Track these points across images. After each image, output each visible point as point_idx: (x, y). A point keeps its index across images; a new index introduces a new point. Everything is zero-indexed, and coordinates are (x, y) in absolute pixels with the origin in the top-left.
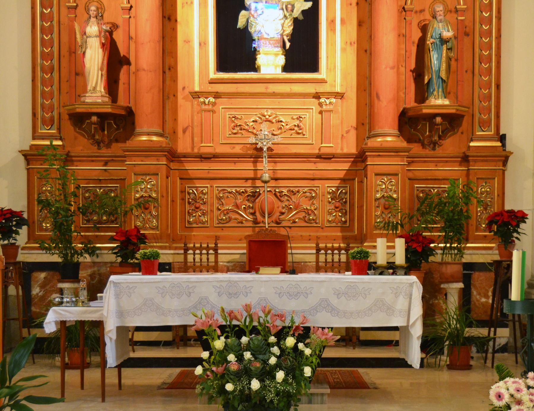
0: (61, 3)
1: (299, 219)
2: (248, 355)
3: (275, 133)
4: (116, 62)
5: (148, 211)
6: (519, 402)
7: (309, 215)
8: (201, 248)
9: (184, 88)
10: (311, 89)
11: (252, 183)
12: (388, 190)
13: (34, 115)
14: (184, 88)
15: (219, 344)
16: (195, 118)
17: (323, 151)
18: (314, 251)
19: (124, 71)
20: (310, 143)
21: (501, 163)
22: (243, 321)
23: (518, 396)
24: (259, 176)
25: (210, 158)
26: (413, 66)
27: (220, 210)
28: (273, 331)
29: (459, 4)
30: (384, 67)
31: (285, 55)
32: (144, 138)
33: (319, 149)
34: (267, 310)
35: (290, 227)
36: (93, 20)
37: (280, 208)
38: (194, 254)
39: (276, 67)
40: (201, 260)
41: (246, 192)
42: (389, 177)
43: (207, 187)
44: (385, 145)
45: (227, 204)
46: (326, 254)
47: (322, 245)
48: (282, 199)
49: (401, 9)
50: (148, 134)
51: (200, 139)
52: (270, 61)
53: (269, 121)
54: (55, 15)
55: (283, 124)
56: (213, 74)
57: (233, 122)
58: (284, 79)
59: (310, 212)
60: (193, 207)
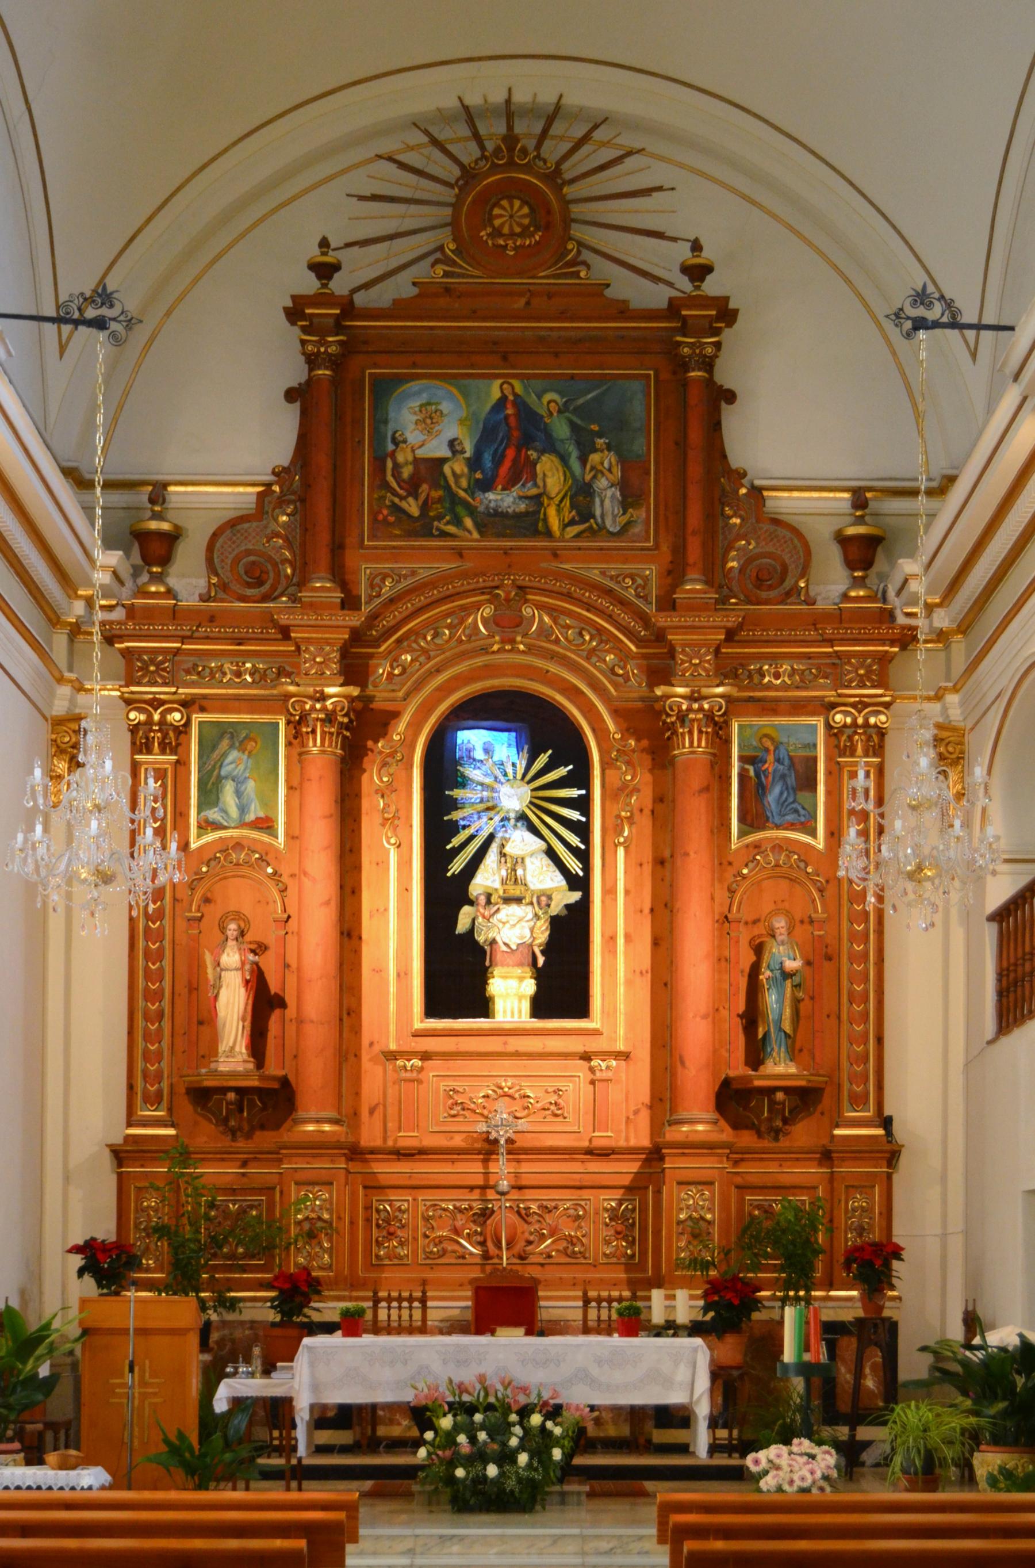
0: (177, 913)
1: (558, 1251)
2: (482, 1436)
3: (518, 1115)
4: (264, 1001)
5: (314, 1242)
6: (778, 1468)
7: (574, 1245)
8: (400, 1299)
9: (371, 1044)
10: (577, 1045)
11: (481, 1194)
12: (699, 1208)
13: (131, 1087)
14: (371, 1044)
15: (446, 1422)
16: (390, 1091)
17: (597, 1143)
18: (580, 1304)
19: (275, 1017)
20: (575, 1129)
21: (885, 1163)
22: (476, 1395)
23: (777, 1461)
24: (491, 1183)
25: (413, 1155)
26: (741, 1007)
27: (428, 1237)
28: (515, 1408)
29: (816, 911)
30: (691, 1015)
31: (535, 979)
32: (311, 1128)
33: (590, 1141)
34: (506, 1382)
35: (542, 1265)
36: (231, 943)
37: (527, 1235)
38: (389, 1308)
39: (521, 998)
40: (400, 1317)
41: (471, 1208)
42: (700, 1188)
43: (408, 1201)
44: (693, 1138)
45: (440, 1228)
46: (599, 1308)
47: (592, 1294)
48: (530, 1219)
49: (722, 919)
50: (318, 1121)
51: (397, 1124)
52: (511, 991)
53: (509, 1096)
54: (167, 932)
55: (532, 1101)
56: (419, 1022)
57: (451, 1097)
58: (533, 1030)
59: (575, 1240)
60: (385, 1233)
